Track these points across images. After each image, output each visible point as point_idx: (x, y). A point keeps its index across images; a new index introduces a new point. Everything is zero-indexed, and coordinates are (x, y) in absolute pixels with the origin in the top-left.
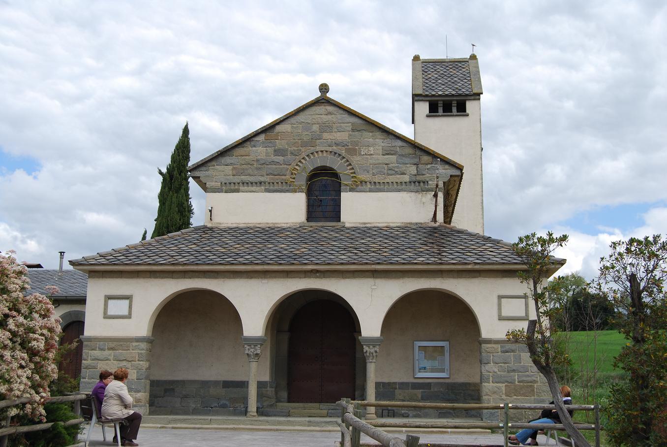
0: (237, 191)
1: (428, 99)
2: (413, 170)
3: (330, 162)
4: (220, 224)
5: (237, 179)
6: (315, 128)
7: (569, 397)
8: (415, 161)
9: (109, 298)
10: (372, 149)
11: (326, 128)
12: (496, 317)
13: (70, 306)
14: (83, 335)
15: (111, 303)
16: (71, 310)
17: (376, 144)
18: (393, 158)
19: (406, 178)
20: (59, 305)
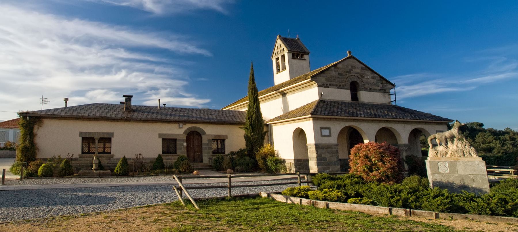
0: (328, 87)
1: (292, 52)
2: (381, 85)
3: (356, 79)
4: (325, 99)
5: (328, 83)
6: (350, 67)
7: (43, 164)
8: (381, 82)
9: (322, 128)
10: (368, 76)
11: (353, 67)
12: (330, 138)
13: (191, 124)
14: (307, 143)
15: (323, 130)
16: (192, 126)
17: (369, 75)
18: (375, 80)
19: (379, 88)
20: (186, 124)
